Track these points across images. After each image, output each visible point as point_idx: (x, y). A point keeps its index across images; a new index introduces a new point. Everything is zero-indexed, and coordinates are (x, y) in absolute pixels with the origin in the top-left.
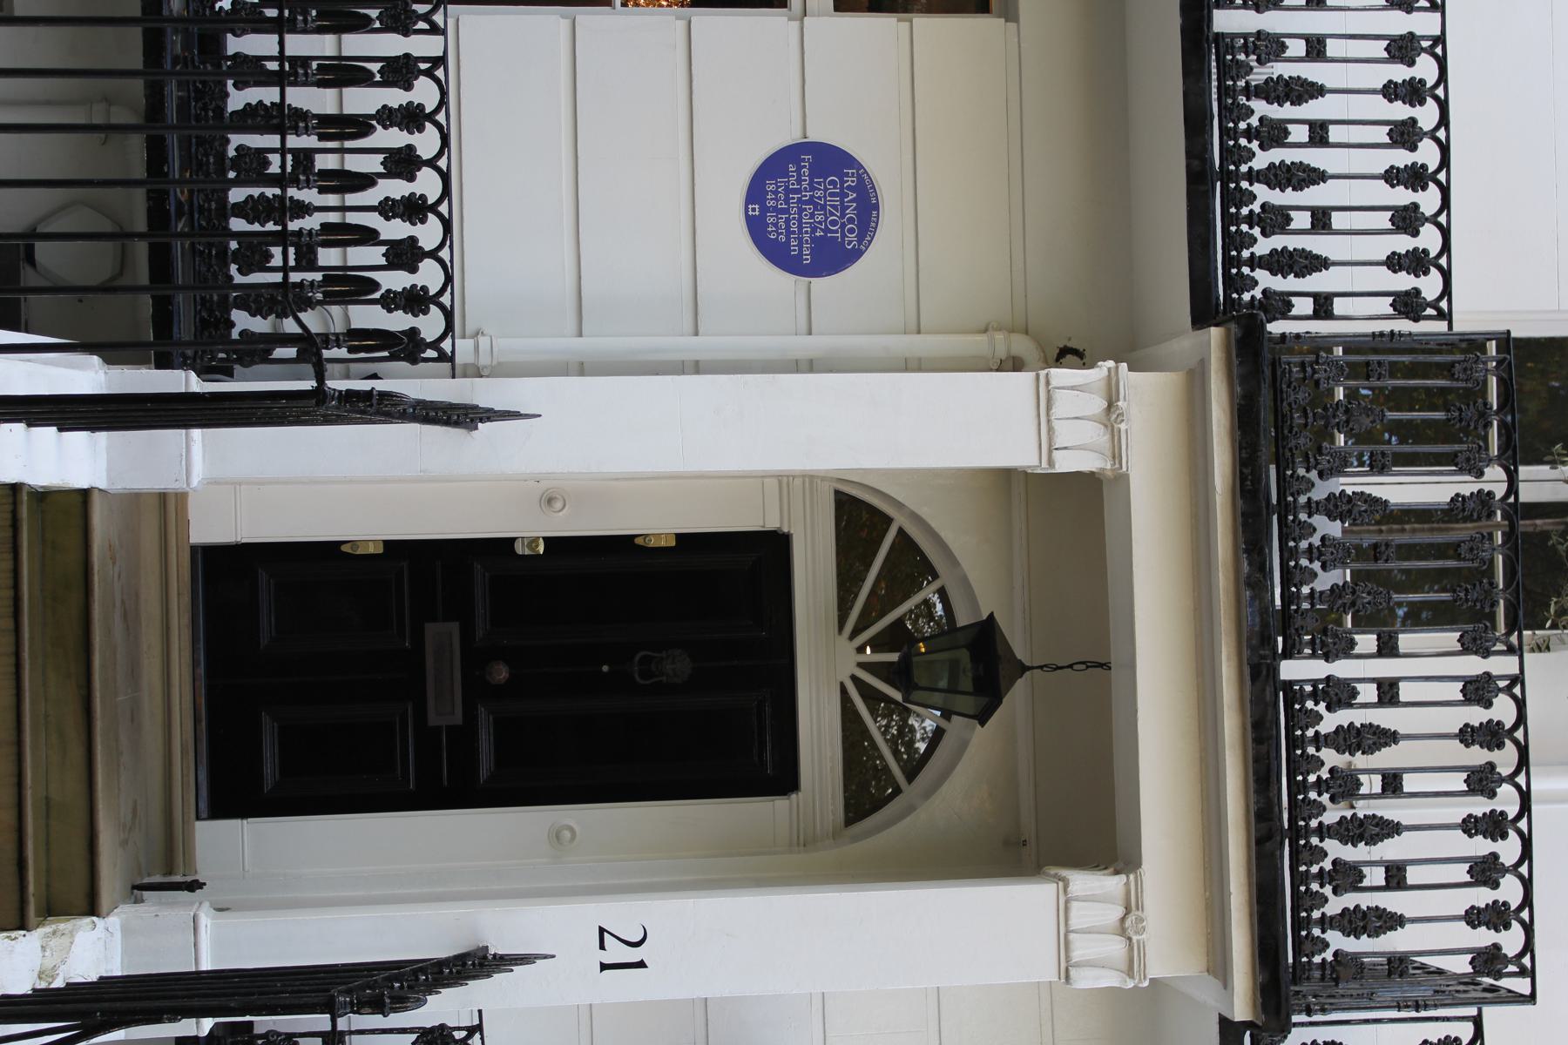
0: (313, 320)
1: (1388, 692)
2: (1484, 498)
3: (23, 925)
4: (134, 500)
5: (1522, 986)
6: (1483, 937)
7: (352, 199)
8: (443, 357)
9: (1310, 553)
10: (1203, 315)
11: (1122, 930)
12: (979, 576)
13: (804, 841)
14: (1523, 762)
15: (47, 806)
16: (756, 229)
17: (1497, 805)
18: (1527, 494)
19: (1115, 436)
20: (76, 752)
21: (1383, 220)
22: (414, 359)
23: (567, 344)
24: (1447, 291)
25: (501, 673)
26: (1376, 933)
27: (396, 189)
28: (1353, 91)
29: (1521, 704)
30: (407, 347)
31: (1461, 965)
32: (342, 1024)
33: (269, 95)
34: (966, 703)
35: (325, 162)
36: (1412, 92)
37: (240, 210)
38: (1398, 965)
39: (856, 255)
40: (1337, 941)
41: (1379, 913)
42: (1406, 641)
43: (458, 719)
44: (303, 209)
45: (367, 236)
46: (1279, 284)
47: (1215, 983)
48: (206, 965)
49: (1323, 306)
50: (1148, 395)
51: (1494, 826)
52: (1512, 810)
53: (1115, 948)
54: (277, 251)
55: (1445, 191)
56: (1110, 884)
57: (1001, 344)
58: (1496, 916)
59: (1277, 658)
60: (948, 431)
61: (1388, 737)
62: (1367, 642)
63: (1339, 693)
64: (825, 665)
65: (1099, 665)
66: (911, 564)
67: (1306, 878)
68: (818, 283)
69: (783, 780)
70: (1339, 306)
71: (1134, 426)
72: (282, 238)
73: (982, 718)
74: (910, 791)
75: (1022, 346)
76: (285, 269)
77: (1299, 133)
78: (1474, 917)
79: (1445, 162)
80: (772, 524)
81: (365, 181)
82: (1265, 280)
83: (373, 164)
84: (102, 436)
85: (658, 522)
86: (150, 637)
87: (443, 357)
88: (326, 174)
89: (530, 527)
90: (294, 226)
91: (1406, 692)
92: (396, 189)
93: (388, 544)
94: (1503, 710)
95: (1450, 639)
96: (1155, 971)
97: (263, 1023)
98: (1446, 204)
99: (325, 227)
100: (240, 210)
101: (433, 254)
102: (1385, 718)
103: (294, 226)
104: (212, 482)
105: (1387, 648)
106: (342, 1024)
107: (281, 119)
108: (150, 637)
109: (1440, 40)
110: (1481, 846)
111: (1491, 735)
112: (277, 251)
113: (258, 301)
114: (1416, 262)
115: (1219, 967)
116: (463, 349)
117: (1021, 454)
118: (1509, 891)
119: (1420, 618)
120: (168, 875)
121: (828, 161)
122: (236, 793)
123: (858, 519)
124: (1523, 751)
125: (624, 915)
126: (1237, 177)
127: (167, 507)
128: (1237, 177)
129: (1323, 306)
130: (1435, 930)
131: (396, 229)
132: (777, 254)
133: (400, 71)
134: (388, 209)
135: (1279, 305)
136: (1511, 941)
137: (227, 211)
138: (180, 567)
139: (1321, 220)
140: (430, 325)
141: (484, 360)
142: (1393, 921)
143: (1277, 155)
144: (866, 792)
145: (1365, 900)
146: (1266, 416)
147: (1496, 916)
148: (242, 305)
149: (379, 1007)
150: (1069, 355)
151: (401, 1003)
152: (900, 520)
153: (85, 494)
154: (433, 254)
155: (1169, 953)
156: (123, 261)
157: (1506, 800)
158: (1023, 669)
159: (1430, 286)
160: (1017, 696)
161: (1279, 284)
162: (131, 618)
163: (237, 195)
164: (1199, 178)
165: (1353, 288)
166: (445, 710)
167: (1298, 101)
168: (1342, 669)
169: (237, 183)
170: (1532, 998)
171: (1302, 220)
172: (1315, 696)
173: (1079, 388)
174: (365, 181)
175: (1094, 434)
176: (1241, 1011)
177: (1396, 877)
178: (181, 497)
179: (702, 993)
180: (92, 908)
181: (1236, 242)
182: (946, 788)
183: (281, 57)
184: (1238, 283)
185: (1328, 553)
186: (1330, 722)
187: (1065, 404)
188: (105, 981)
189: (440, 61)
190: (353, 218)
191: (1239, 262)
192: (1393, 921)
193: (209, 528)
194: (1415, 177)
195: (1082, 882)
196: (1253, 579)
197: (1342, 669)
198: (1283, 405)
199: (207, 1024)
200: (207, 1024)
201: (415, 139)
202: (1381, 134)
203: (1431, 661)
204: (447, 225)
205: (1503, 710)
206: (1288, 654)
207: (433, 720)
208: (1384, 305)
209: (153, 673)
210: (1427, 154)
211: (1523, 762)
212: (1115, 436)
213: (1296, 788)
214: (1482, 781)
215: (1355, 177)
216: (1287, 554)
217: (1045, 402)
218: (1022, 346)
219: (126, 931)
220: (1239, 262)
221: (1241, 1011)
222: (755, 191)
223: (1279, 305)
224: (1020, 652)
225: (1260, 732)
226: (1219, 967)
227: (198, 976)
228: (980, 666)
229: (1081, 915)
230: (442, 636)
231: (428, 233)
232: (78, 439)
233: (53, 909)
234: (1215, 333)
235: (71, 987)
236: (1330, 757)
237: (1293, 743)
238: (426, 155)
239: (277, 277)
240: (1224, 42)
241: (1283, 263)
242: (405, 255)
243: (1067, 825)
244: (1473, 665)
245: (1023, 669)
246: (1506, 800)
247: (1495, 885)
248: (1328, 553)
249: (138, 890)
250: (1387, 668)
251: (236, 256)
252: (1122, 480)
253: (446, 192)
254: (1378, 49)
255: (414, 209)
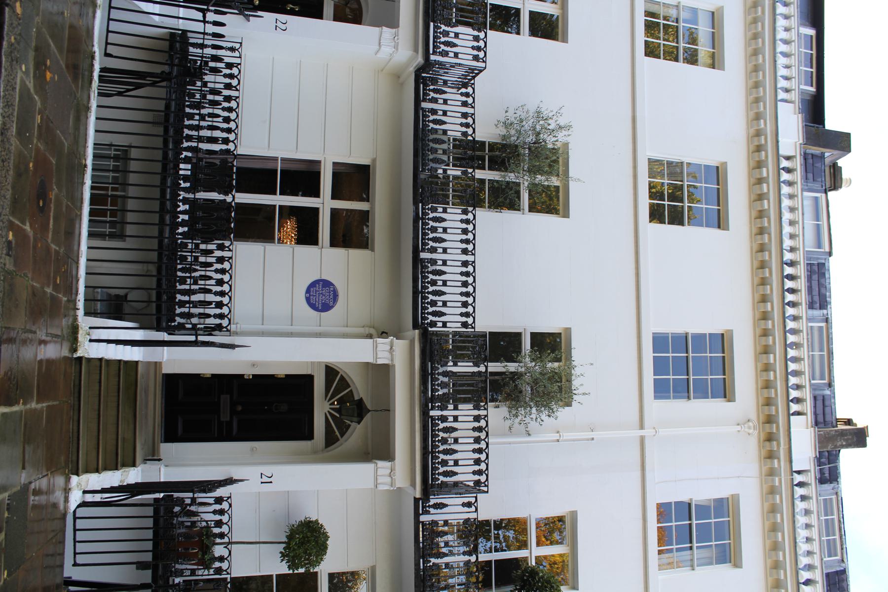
0: (203, 111)
1: (456, 419)
2: (480, 372)
3: (117, 469)
4: (149, 363)
5: (485, 489)
6: (477, 477)
7: (215, 119)
8: (228, 330)
9: (438, 385)
10: (415, 326)
11: (390, 476)
12: (360, 388)
13: (315, 452)
14: (487, 435)
15: (124, 439)
16: (308, 300)
17: (481, 467)
18: (490, 370)
19: (392, 355)
20: (132, 426)
21: (459, 304)
22: (220, 331)
23: (259, 327)
24: (474, 322)
25: (240, 408)
26: (451, 476)
27: (219, 266)
28: (453, 273)
29: (487, 422)
30: (219, 327)
31: (471, 484)
32: (196, 495)
33: (195, 144)
34: (356, 419)
35: (203, 247)
36: (467, 274)
37: (180, 270)
38: (456, 484)
39: (333, 307)
40: (442, 478)
41: (452, 472)
42: (460, 407)
43: (228, 419)
44: (196, 270)
45: (210, 278)
46: (434, 319)
47: (412, 488)
48: (162, 480)
49: (444, 324)
50: (400, 346)
51: (480, 451)
52: (471, 123)
53: (388, 480)
54: (188, 280)
55: (474, 278)
56: (387, 464)
57: (367, 331)
58: (480, 472)
59: (429, 410)
60: (352, 353)
61: (455, 430)
62: (451, 407)
63: (444, 419)
64: (321, 409)
65: (387, 410)
66: (344, 383)
67: (435, 441)
68: (322, 314)
69: (310, 436)
70: (448, 325)
71: (398, 354)
72: (190, 277)
73: (359, 423)
74: (342, 440)
75: (372, 331)
76: (190, 284)
77: (440, 283)
78: (474, 473)
79: (474, 238)
80: (309, 373)
81: (210, 265)
82: (431, 318)
83: (213, 260)
84: (142, 348)
85: (281, 371)
86: (151, 397)
87: (228, 330)
88: (202, 263)
89: (248, 372)
90: (193, 275)
91: (460, 419)
92: (219, 266)
93: (212, 375)
94: (483, 423)
95: (471, 406)
96: (398, 485)
97: (176, 495)
98: (474, 301)
99: (201, 276)
100: (180, 270)
101: (233, 142)
102: (455, 425)
103: (193, 275)
104: (168, 360)
105: (456, 408)
106: (196, 495)
107: (189, 316)
108: (151, 397)
109: (474, 262)
110: (477, 456)
111: (480, 429)
112: (188, 280)
113: (191, 127)
114: (467, 315)
115: (413, 485)
116: (233, 327)
117: (370, 359)
118: (483, 466)
119: (466, 401)
120: (153, 456)
121: (327, 284)
122: (171, 436)
123: (331, 372)
124: (487, 433)
125: (267, 470)
126: (425, 293)
127: (157, 365)
128: (425, 293)
129: (444, 324)
130: (464, 474)
131: (219, 276)
132: (313, 306)
133: (220, 305)
134: (217, 271)
135: (433, 324)
136: (483, 478)
137: (176, 270)
138: (159, 379)
139: (445, 304)
140: (225, 323)
141: (238, 330)
142: (455, 474)
143: (434, 288)
144: (331, 440)
145: (437, 288)
146: (428, 352)
147: (480, 472)
148: (188, 106)
149: (205, 491)
150: (383, 334)
151: (210, 491)
152: (341, 373)
153: (137, 362)
154: (233, 142)
155: (402, 481)
156: (150, 296)
157: (483, 445)
158: (369, 411)
159: (470, 320)
160: (368, 418)
161: (434, 319)
162: (146, 391)
163: (179, 267)
164: (415, 293)
165: (452, 320)
166: (225, 417)
167: (440, 275)
168: (445, 413)
169: (180, 264)
170: (487, 492)
171: (440, 304)
172: (438, 419)
173: (383, 343)
174: (210, 265)
175: (387, 355)
176: (418, 495)
177: (456, 463)
178: (160, 363)
179: (286, 489)
180: (134, 465)
181: (424, 234)
182: (350, 440)
183: (189, 307)
184: (424, 318)
185: (444, 385)
186: (442, 426)
187: (380, 347)
188: (136, 483)
189: (231, 258)
190: (215, 124)
191: (424, 313)
192: (455, 474)
193: (166, 370)
194: (467, 294)
195: (381, 463)
196: (424, 391)
197: (445, 413)
198: (432, 349)
199: (162, 495)
200: (162, 495)
201: (230, 115)
202: (459, 284)
203: (466, 411)
204: (230, 298)
205: (483, 423)
206: (432, 409)
207: (222, 419)
208: (459, 325)
209: (152, 405)
210: (470, 236)
211: (487, 435)
212: (392, 355)
213: (433, 441)
214: (477, 440)
215: (453, 294)
216: (432, 385)
217: (375, 347)
218: (372, 331)
219: (142, 471)
220: (424, 313)
221: (418, 495)
222: (308, 291)
223: (433, 324)
224: (369, 407)
225: (424, 428)
226: (413, 485)
227: (160, 483)
228: (359, 410)
229: (380, 472)
230: (225, 399)
231: (226, 300)
232: (136, 349)
233: (124, 465)
234: (417, 331)
235: (128, 485)
236: (441, 434)
237: (432, 431)
238: (225, 325)
239: (197, 123)
240: (423, 260)
241: (435, 314)
242: (220, 282)
243: (379, 450)
244: (476, 412)
245: (369, 411)
246: (483, 445)
247: (479, 444)
248: (444, 385)
249: (145, 460)
250: (456, 413)
251: (179, 281)
252: (394, 366)
253: (231, 290)
254: (459, 264)
255: (230, 110)
